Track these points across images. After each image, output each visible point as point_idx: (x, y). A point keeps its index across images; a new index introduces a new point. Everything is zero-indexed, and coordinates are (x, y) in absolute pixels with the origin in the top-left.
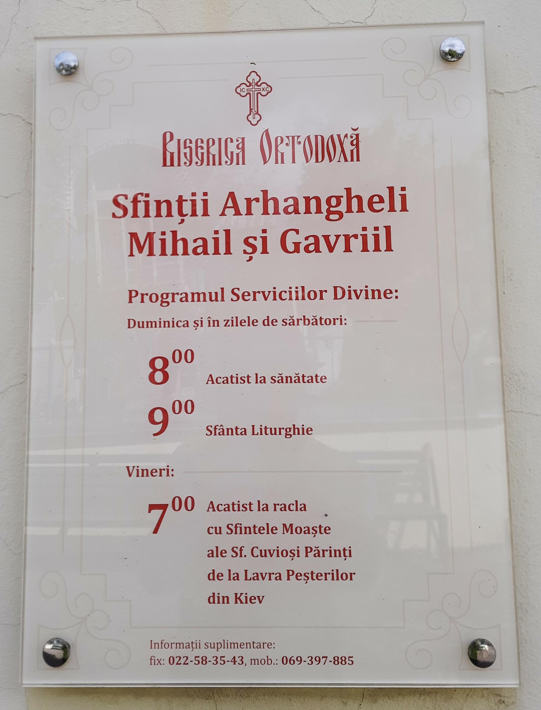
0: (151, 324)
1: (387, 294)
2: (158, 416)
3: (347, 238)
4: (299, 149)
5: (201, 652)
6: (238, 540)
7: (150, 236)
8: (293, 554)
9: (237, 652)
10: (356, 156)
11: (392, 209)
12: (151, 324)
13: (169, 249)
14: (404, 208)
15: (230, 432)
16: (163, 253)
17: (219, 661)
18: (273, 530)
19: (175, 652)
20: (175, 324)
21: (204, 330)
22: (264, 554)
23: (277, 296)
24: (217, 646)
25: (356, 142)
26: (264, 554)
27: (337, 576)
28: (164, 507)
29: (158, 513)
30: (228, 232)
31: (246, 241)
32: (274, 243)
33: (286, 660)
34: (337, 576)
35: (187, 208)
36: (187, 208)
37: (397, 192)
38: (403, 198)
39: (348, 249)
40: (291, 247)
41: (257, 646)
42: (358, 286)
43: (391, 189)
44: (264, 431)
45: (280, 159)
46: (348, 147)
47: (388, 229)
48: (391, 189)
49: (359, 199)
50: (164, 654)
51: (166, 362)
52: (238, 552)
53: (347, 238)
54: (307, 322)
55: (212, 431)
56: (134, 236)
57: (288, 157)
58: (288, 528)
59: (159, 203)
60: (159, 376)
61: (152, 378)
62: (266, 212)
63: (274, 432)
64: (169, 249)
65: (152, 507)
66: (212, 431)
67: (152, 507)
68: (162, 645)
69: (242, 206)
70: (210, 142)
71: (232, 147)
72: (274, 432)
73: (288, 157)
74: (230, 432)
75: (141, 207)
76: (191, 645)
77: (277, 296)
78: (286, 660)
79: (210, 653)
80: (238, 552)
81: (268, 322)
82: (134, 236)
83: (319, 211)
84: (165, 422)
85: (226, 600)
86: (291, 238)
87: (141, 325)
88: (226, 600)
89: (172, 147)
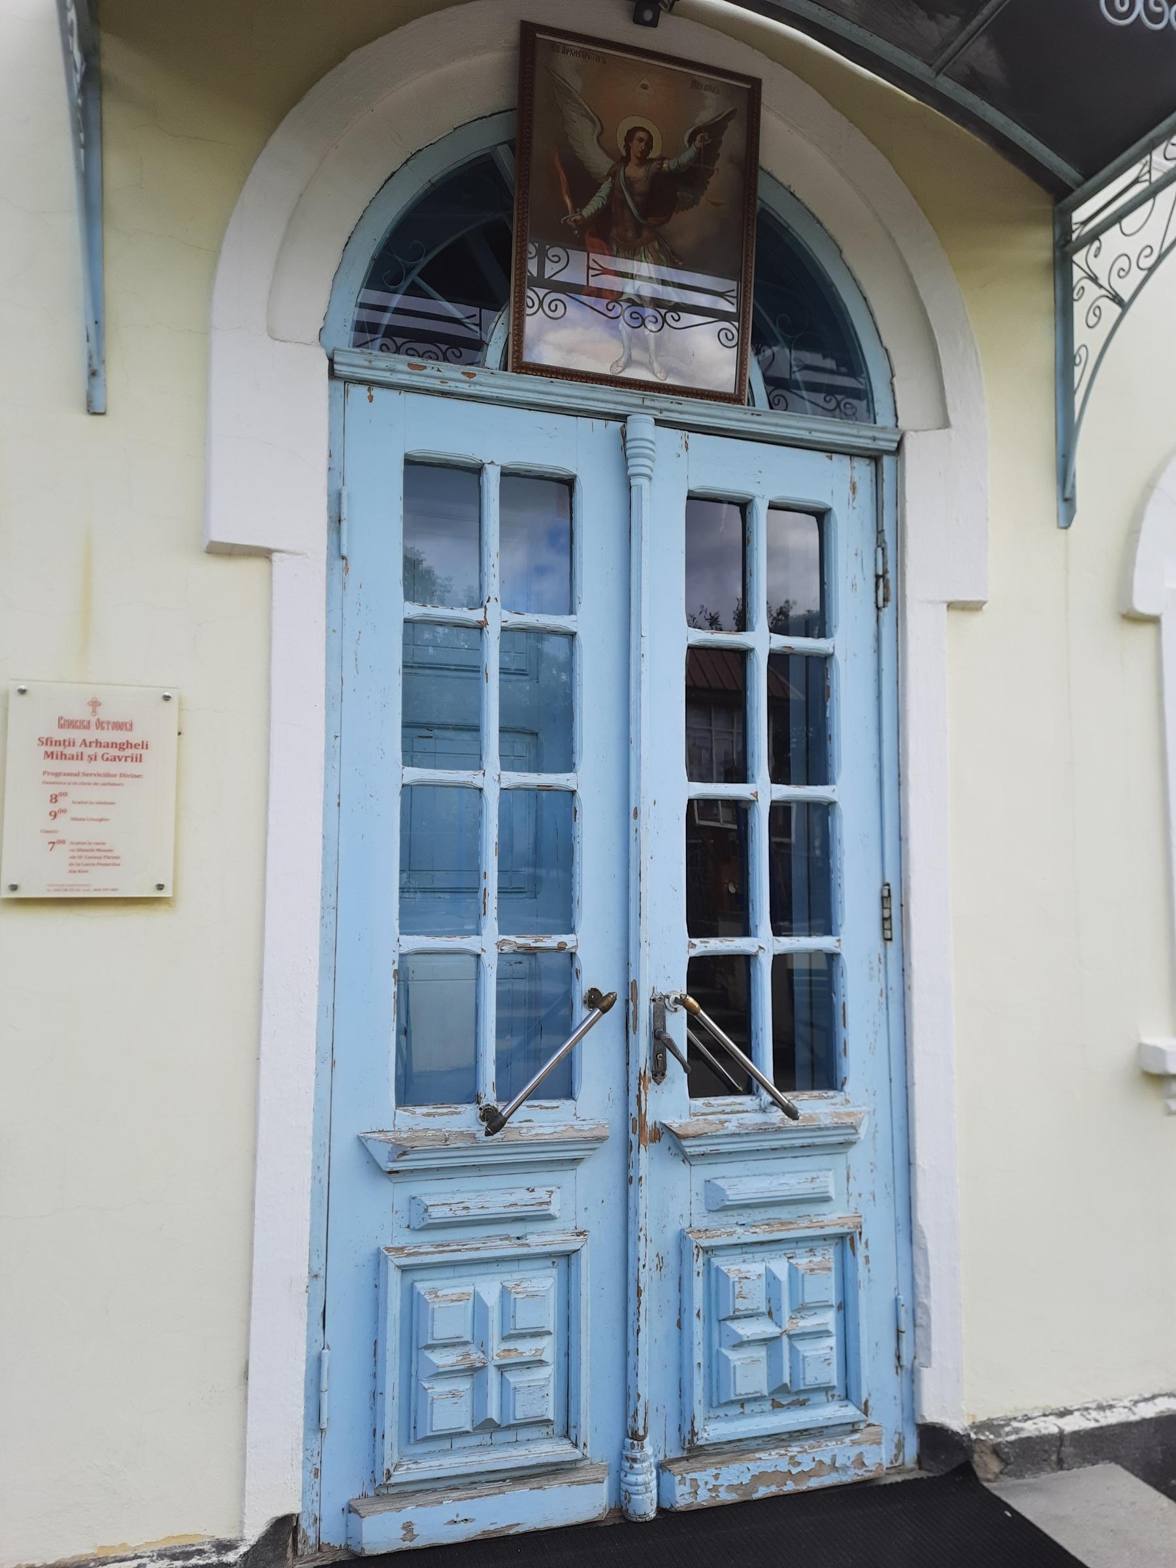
0: (51, 783)
1: (139, 776)
2: (53, 814)
3: (126, 757)
4: (110, 726)
5: (65, 888)
6: (80, 853)
7: (52, 753)
8: (100, 858)
9: (77, 888)
10: (131, 730)
11: (143, 748)
12: (51, 783)
13: (59, 757)
14: (147, 748)
15: (79, 820)
16: (57, 758)
17: (72, 890)
18: (85, 857)
19: (56, 888)
20: (61, 783)
21: (71, 786)
22: (90, 858)
23: (99, 775)
24: (71, 886)
25: (131, 725)
26: (90, 858)
27: (114, 865)
28: (54, 843)
29: (51, 845)
30: (82, 753)
31: (89, 756)
32: (99, 757)
33: (95, 890)
34: (114, 865)
35: (67, 743)
36: (67, 743)
37: (117, 861)
38: (147, 745)
39: (126, 760)
40: (105, 759)
41: (557, 262)
42: (129, 773)
43: (143, 742)
44: (92, 819)
45: (103, 728)
46: (128, 727)
47: (141, 755)
48: (143, 742)
49: (131, 744)
50: (52, 888)
51: (56, 796)
52: (80, 857)
53: (126, 757)
54: (99, 745)
55: (74, 819)
56: (46, 752)
57: (106, 728)
58: (98, 850)
59: (56, 742)
60: (54, 801)
61: (51, 801)
62: (96, 746)
63: (96, 820)
64: (59, 757)
65: (50, 843)
66: (74, 819)
67: (50, 843)
68: (51, 885)
69: (88, 744)
70: (77, 721)
71: (85, 723)
72: (96, 820)
73: (106, 728)
74: (79, 820)
75: (49, 742)
76: (63, 885)
77: (99, 775)
78: (95, 890)
79: (68, 888)
80: (80, 857)
81: (96, 784)
82: (46, 752)
83: (116, 747)
84: (55, 816)
85: (75, 872)
86: (105, 756)
87: (47, 783)
88: (75, 872)
89: (62, 722)
